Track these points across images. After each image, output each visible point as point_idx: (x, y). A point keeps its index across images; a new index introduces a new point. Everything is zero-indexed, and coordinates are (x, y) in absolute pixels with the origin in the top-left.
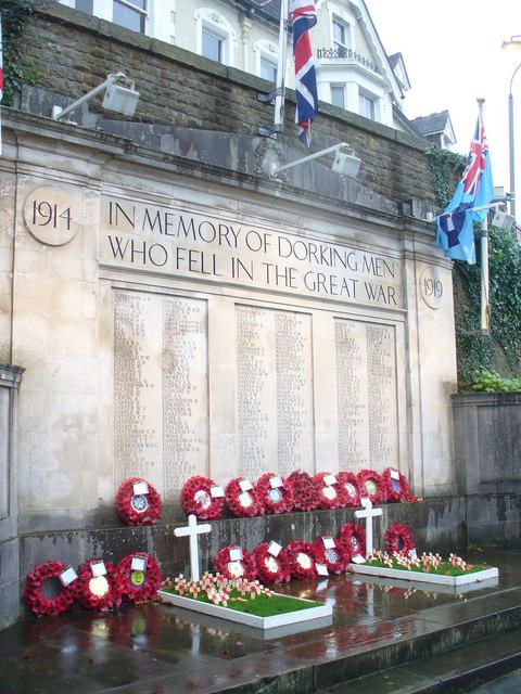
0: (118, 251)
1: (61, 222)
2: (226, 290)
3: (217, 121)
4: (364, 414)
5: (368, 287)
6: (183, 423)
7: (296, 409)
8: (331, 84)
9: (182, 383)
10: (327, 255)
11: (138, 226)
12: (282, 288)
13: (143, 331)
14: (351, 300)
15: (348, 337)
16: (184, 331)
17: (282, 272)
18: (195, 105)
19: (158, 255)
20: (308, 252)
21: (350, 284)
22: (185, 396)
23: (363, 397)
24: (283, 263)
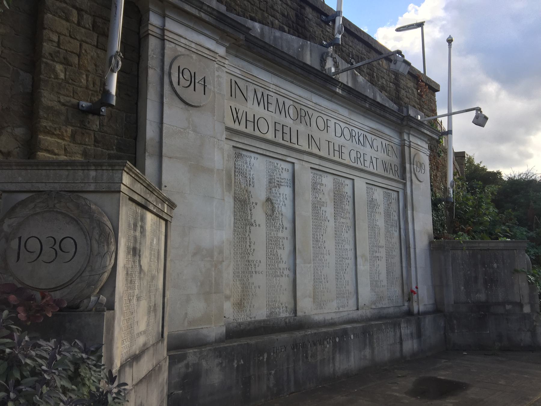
0: (237, 120)
2: (306, 158)
5: (384, 163)
6: (279, 255)
9: (278, 224)
10: (361, 139)
11: (250, 101)
12: (337, 158)
13: (253, 182)
14: (375, 171)
16: (279, 186)
18: (283, 15)
19: (262, 125)
20: (351, 136)
21: (374, 160)
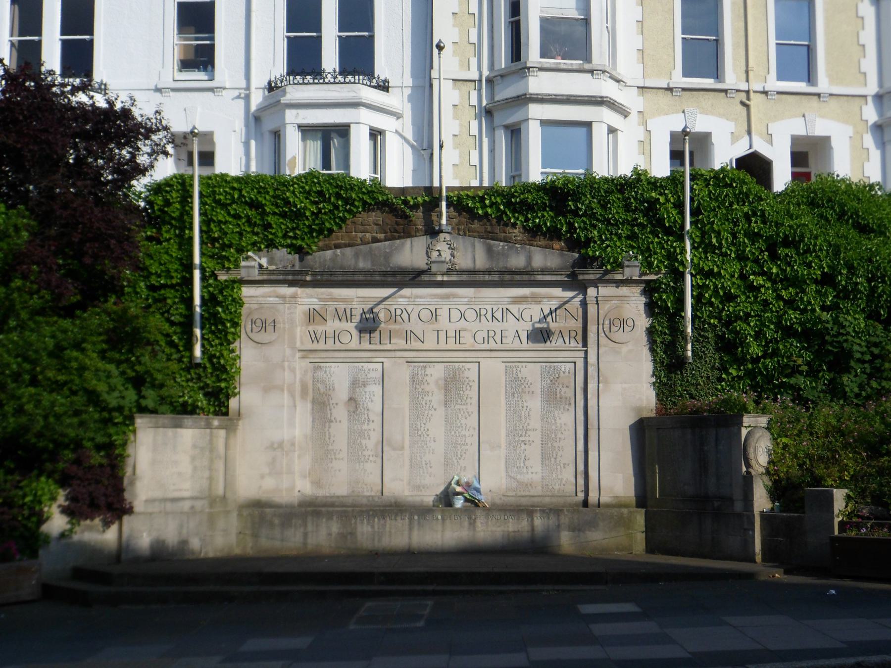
0: (315, 339)
1: (270, 328)
2: (398, 354)
3: (396, 231)
4: (536, 437)
7: (463, 433)
8: (299, 126)
15: (520, 376)
17: (451, 334)
22: (365, 427)
23: (535, 422)
24: (452, 328)
